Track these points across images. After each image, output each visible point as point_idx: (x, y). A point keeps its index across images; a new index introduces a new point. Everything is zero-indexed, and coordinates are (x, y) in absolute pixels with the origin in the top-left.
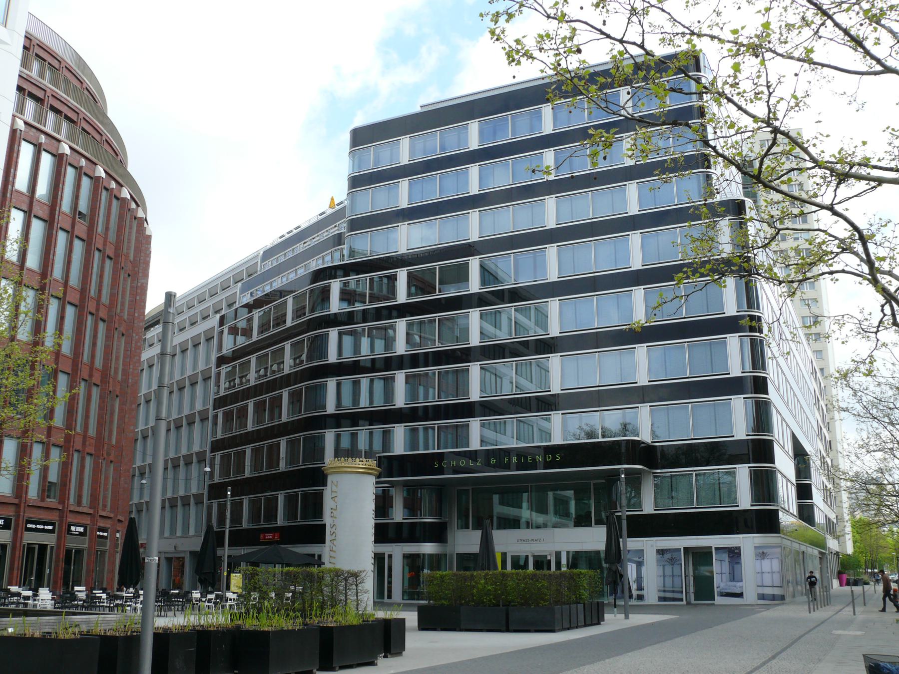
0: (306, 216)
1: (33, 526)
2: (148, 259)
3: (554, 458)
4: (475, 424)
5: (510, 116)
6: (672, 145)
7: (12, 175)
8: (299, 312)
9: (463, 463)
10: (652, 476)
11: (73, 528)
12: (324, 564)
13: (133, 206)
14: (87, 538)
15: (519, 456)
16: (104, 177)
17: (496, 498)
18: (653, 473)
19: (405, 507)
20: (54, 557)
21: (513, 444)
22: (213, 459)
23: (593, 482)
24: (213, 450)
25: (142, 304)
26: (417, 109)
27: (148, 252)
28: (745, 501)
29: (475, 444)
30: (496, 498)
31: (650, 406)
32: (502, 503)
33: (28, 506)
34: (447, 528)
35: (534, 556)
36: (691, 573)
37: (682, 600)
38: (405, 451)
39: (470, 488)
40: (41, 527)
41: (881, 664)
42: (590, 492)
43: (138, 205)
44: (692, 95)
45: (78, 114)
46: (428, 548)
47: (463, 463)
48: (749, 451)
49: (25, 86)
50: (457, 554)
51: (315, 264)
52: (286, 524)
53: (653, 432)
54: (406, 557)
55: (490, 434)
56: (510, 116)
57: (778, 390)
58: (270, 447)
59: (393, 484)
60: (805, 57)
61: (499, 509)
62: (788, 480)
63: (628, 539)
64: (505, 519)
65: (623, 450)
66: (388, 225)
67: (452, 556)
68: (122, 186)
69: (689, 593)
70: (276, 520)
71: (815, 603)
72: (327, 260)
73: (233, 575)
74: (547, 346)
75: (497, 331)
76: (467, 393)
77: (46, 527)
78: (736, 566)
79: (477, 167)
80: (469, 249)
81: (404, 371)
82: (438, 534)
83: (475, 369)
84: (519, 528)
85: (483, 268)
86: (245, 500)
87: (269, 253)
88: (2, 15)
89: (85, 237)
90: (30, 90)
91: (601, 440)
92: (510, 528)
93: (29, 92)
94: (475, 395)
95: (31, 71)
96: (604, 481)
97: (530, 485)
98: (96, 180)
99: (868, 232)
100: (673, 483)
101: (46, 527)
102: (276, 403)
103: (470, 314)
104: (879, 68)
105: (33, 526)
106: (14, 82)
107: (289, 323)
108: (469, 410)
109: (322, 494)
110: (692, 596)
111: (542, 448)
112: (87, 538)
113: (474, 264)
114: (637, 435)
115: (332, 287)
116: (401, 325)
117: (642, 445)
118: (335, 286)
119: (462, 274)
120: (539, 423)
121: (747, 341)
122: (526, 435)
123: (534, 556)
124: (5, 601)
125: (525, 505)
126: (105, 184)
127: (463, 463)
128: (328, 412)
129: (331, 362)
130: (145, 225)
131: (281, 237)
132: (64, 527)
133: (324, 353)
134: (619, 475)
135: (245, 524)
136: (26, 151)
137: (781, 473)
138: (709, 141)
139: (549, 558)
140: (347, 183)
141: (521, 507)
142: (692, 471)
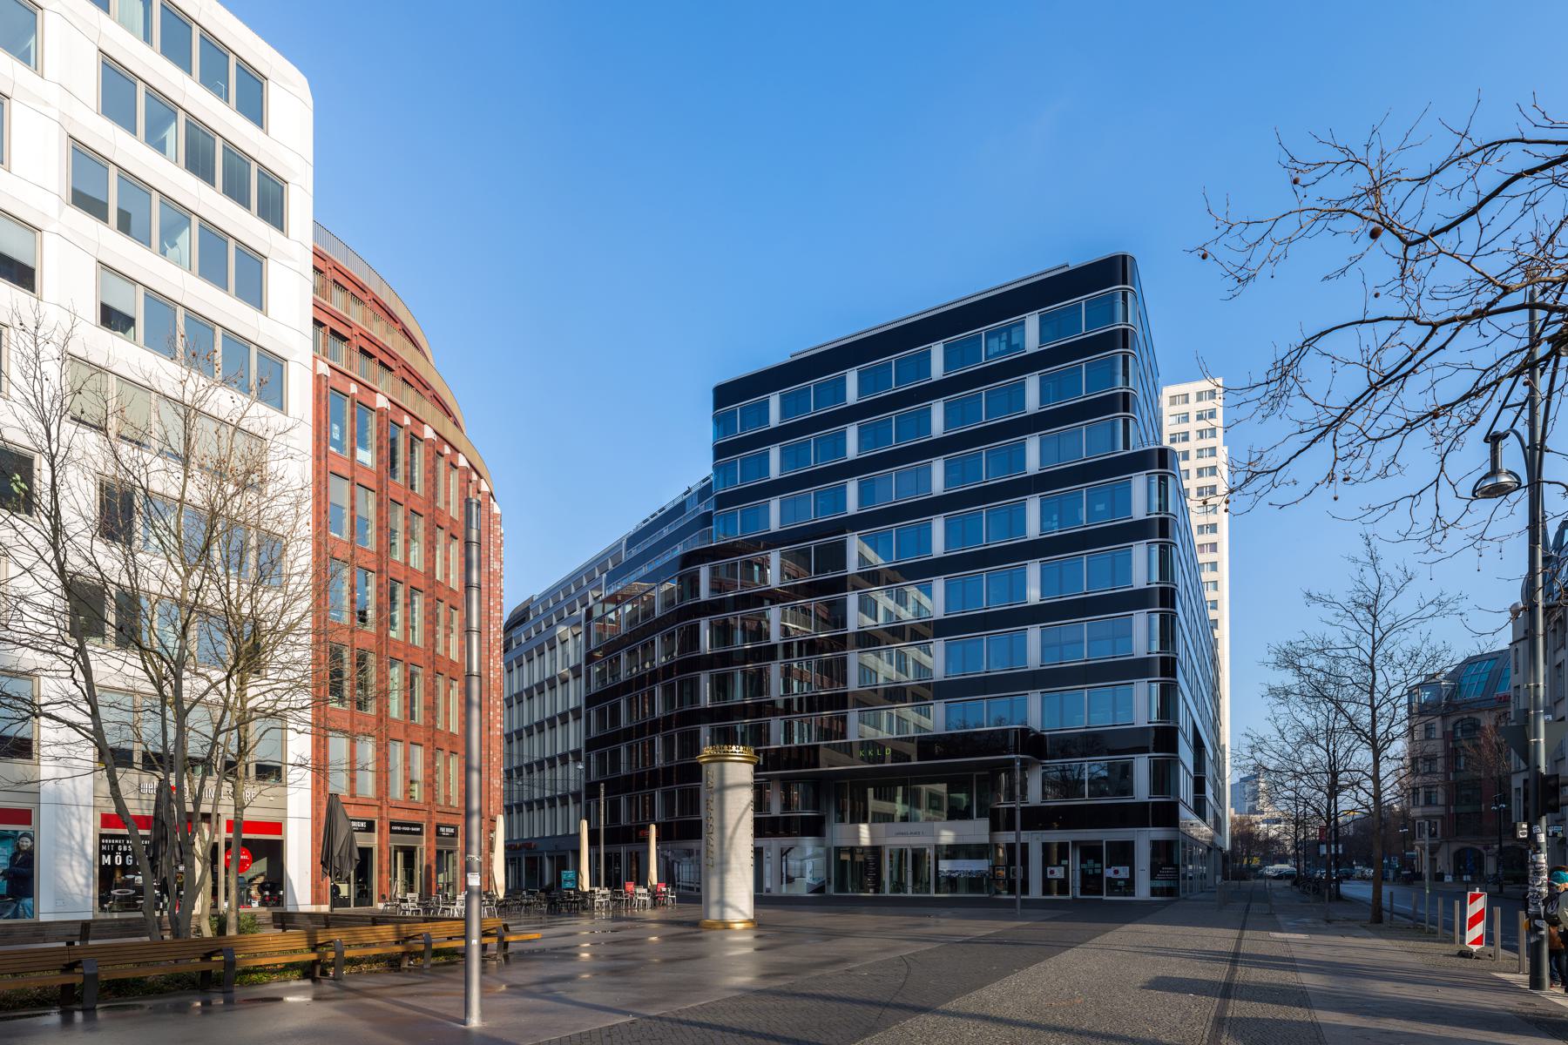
0: (669, 496)
1: (399, 828)
5: (1084, 427)
10: (1040, 766)
11: (442, 829)
13: (474, 477)
14: (424, 837)
15: (242, 889)
16: (329, 375)
17: (871, 791)
20: (634, 758)
22: (588, 759)
23: (975, 774)
24: (588, 749)
26: (786, 359)
28: (1142, 789)
30: (871, 791)
35: (913, 850)
36: (1078, 867)
37: (809, 741)
40: (408, 829)
42: (972, 785)
43: (480, 477)
44: (463, 987)
49: (324, 318)
51: (679, 550)
54: (1156, 845)
56: (1084, 427)
57: (1184, 673)
59: (769, 778)
60: (1025, 766)
61: (873, 804)
62: (1188, 772)
64: (879, 814)
69: (406, 464)
71: (515, 795)
72: (694, 544)
73: (1495, 872)
74: (941, 628)
76: (1023, 531)
77: (413, 829)
79: (1038, 565)
81: (1038, 434)
84: (755, 837)
87: (633, 540)
89: (332, 478)
92: (281, 54)
93: (331, 329)
99: (1365, 596)
100: (1528, 179)
101: (413, 829)
103: (1134, 617)
104: (1481, 244)
105: (399, 828)
106: (309, 313)
107: (657, 614)
109: (698, 791)
110: (1078, 890)
111: (916, 741)
112: (376, 835)
115: (1027, 383)
118: (704, 572)
121: (1156, 548)
122: (58, 958)
123: (913, 850)
124: (113, 860)
125: (899, 799)
126: (392, 417)
128: (934, 380)
129: (1138, 657)
130: (78, 578)
131: (644, 522)
132: (433, 829)
134: (1014, 764)
135: (623, 821)
137: (1183, 764)
138: (312, 724)
140: (712, 452)
141: (894, 801)
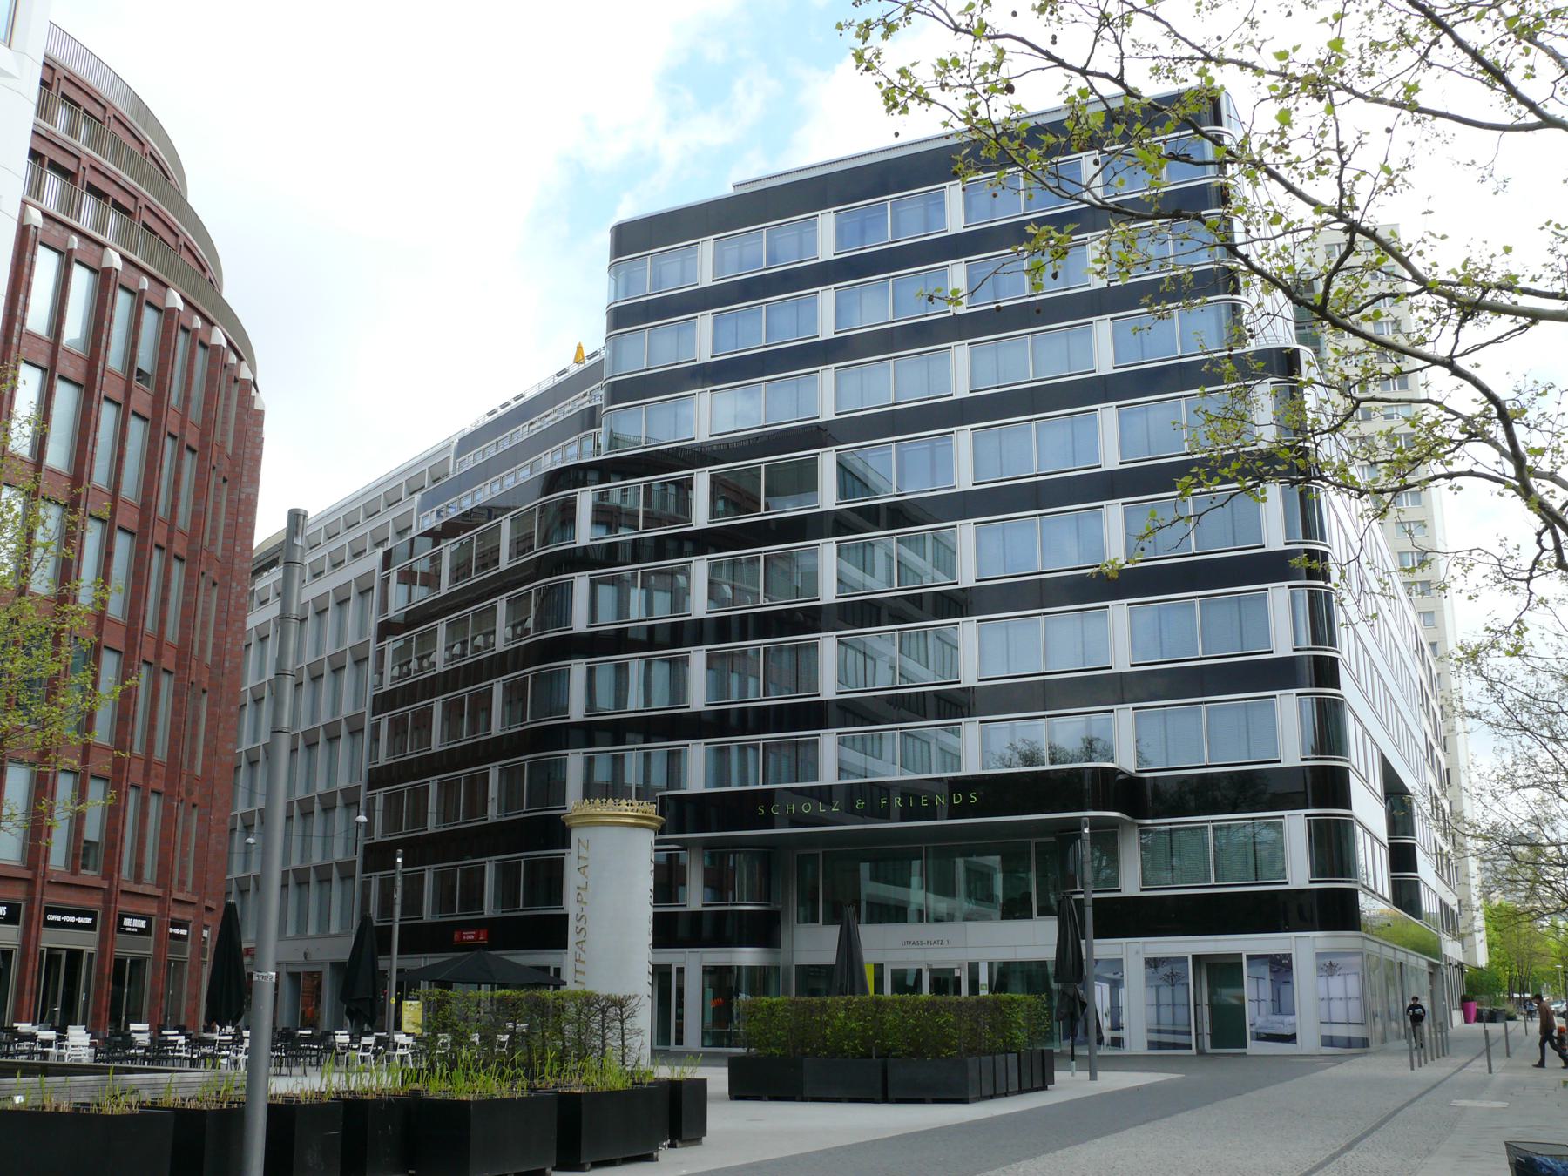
0: (534, 378)
1: (58, 918)
2: (258, 452)
3: (967, 798)
4: (829, 740)
5: (889, 203)
6: (1171, 253)
7: (20, 305)
8: (521, 544)
9: (807, 808)
10: (1137, 831)
11: (127, 922)
12: (565, 983)
13: (233, 359)
14: (152, 938)
15: (905, 796)
16: (182, 309)
17: (865, 869)
18: (1140, 825)
19: (706, 885)
20: (94, 972)
21: (894, 775)
22: (371, 802)
23: (1034, 841)
24: (371, 785)
25: (248, 530)
26: (727, 190)
27: (258, 440)
28: (1299, 873)
29: (828, 775)
30: (865, 869)
31: (1134, 709)
32: (875, 878)
33: (49, 882)
34: (779, 922)
35: (932, 971)
36: (1205, 1000)
37: (1189, 1047)
38: (706, 787)
39: (820, 851)
40: (72, 919)
41: (1537, 1158)
42: (1030, 859)
43: (240, 358)
44: (1207, 166)
45: (136, 198)
46: (747, 957)
47: (807, 807)
48: (1306, 787)
49: (44, 149)
50: (797, 967)
51: (550, 461)
52: (499, 914)
53: (1139, 754)
54: (709, 971)
55: (855, 758)
56: (889, 203)
57: (1357, 680)
58: (471, 780)
59: (685, 845)
60: (1404, 100)
61: (870, 888)
62: (1374, 838)
63: (1096, 941)
64: (881, 905)
65: (1087, 785)
66: (676, 392)
67: (788, 970)
68: (212, 324)
69: (1202, 1034)
70: (481, 907)
71: (1422, 1053)
72: (571, 453)
73: (406, 1003)
74: (954, 604)
75: (868, 577)
76: (814, 685)
77: (81, 920)
78: (1284, 988)
79: (832, 292)
80: (818, 435)
81: (705, 647)
82: (763, 931)
83: (828, 644)
84: (906, 922)
85: (843, 468)
86: (427, 873)
87: (468, 442)
88: (4, 25)
89: (148, 414)
90: (52, 158)
91: (1048, 767)
92: (889, 922)
93: (50, 160)
94: (828, 689)
95: (54, 123)
96: (1053, 839)
97: (924, 846)
98: (167, 314)
99: (1514, 405)
100: (1174, 843)
101: (81, 920)
102: (482, 702)
103: (820, 548)
104: (1533, 118)
105: (58, 918)
106: (25, 142)
107: (504, 563)
108: (817, 715)
109: (561, 862)
110: (1207, 1040)
111: (946, 781)
112: (152, 938)
113: (827, 460)
114: (1111, 759)
115: (578, 500)
116: (700, 567)
117: (1121, 777)
118: (585, 500)
119: (805, 479)
120: (939, 738)
121: (1303, 595)
122: (918, 758)
123: (932, 971)
124: (8, 1048)
125: (915, 881)
126: (183, 321)
127: (807, 807)
128: (572, 720)
129: (577, 632)
130: (254, 392)
131: (489, 414)
132: (112, 920)
133: (565, 617)
134: (1080, 829)
135: (428, 915)
136: (46, 264)
137: (1362, 825)
138: (1236, 245)
139: (957, 973)
140: (605, 318)
141: (908, 885)
142: (1208, 821)
